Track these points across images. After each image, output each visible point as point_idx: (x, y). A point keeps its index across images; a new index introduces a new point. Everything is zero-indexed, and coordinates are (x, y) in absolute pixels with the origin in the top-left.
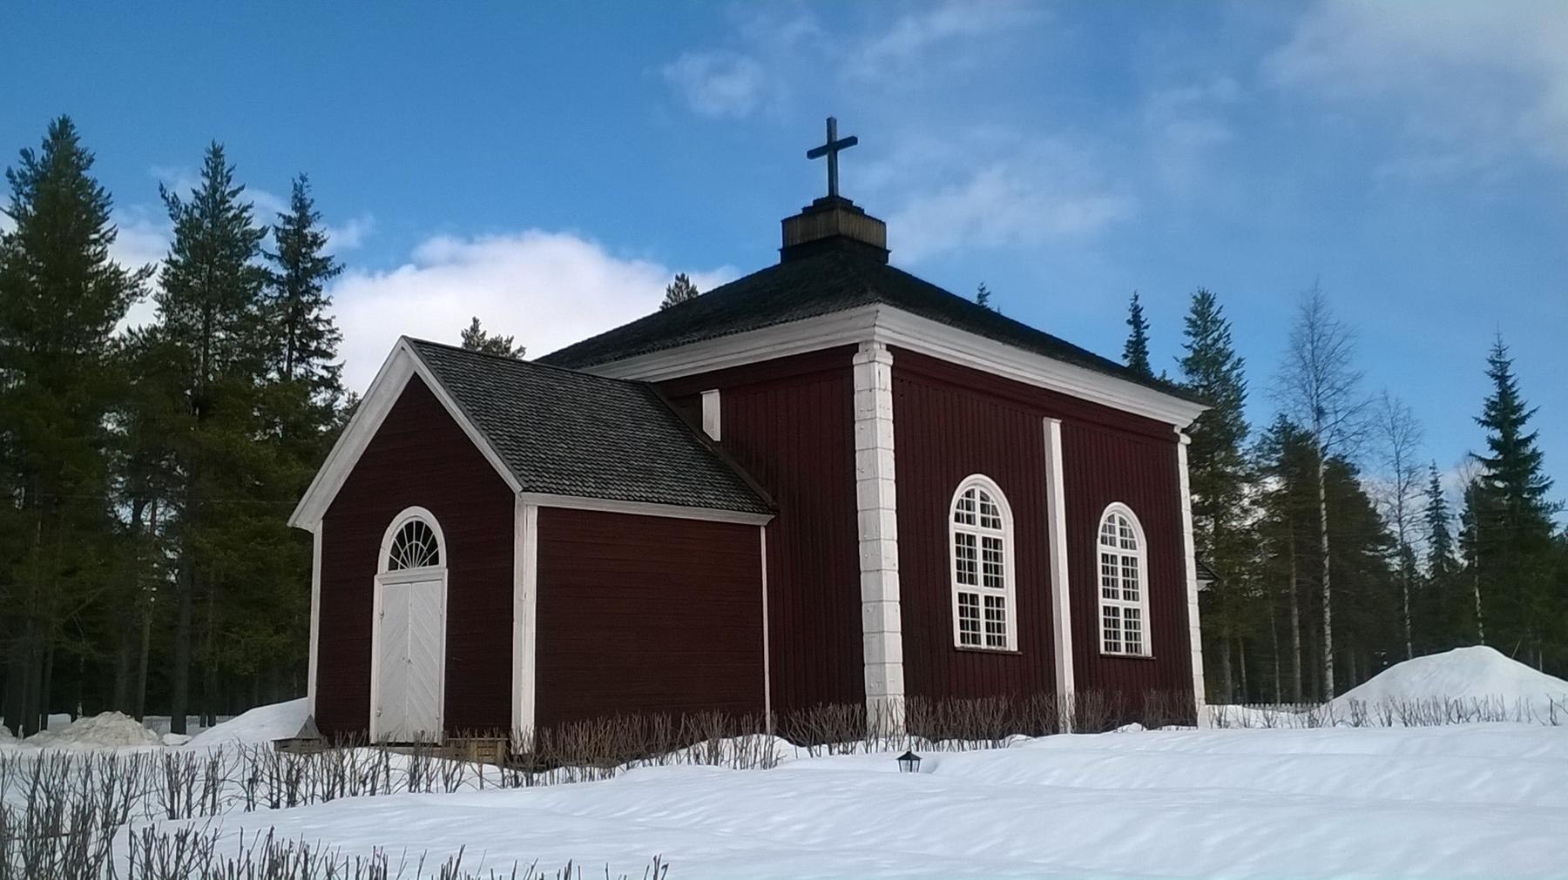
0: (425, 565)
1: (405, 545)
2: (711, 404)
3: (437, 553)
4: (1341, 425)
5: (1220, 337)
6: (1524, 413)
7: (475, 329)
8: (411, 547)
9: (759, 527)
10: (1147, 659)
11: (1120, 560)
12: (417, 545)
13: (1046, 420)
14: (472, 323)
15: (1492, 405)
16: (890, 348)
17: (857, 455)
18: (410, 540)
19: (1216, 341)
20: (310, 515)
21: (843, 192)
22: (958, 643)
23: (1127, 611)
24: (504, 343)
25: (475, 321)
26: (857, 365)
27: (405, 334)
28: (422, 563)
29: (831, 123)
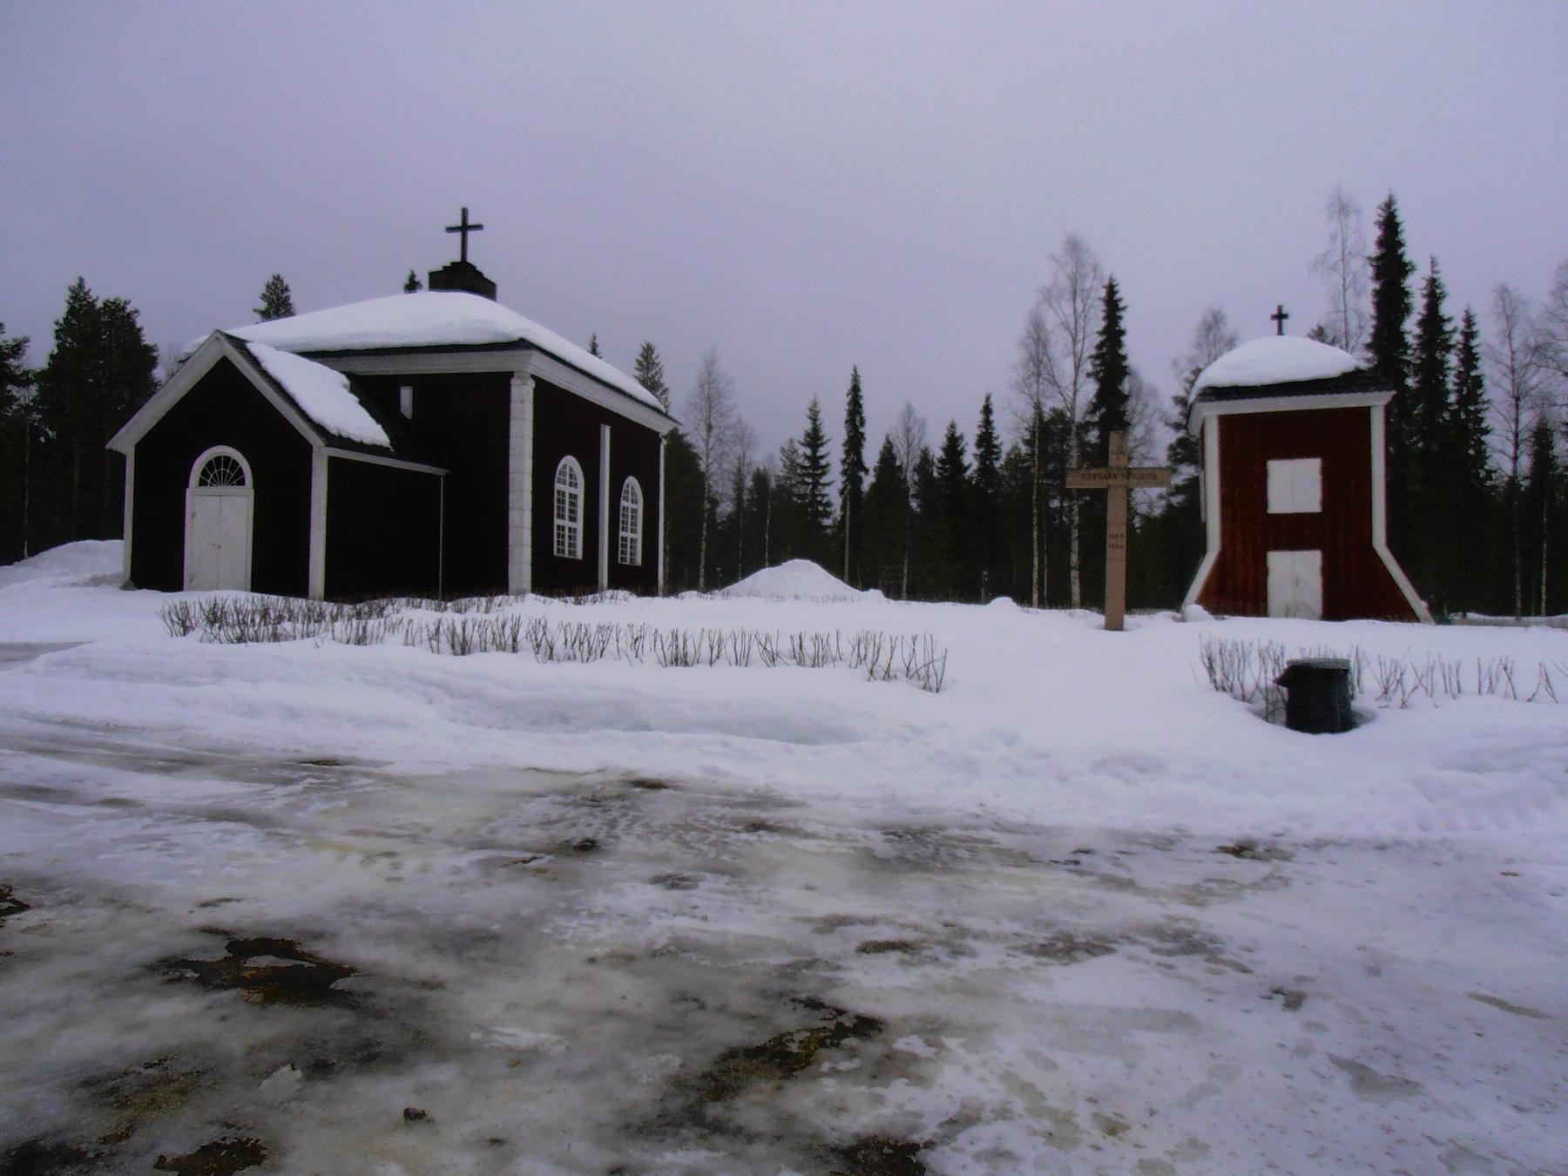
0: (233, 485)
2: (406, 395)
4: (721, 436)
5: (656, 373)
6: (824, 440)
7: (81, 286)
9: (440, 476)
10: (638, 567)
11: (630, 510)
12: (225, 472)
13: (602, 425)
14: (79, 282)
15: (808, 435)
16: (534, 377)
18: (219, 467)
19: (653, 376)
20: (125, 441)
21: (471, 259)
22: (555, 554)
23: (632, 540)
24: (122, 304)
25: (81, 280)
27: (220, 329)
28: (231, 483)
29: (465, 212)
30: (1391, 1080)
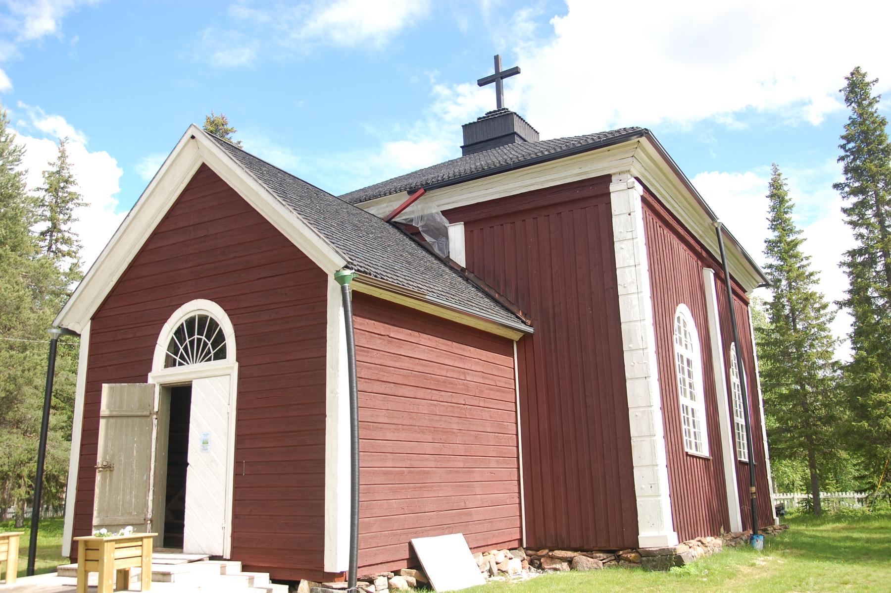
0: (209, 360)
1: (186, 340)
3: (225, 346)
8: (192, 343)
12: (199, 340)
17: (618, 272)
18: (191, 334)
26: (613, 192)
28: (206, 358)
30: (408, 176)
